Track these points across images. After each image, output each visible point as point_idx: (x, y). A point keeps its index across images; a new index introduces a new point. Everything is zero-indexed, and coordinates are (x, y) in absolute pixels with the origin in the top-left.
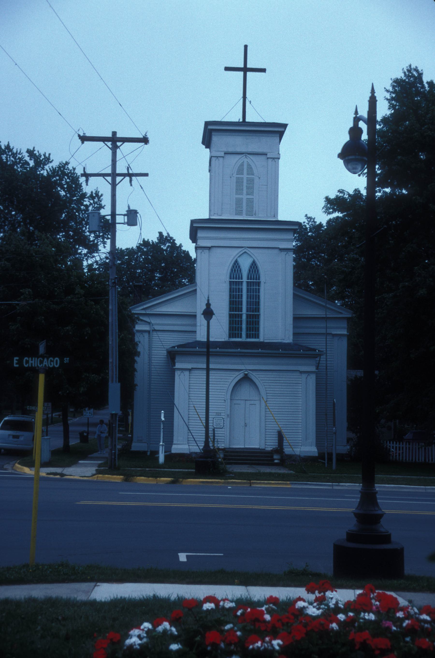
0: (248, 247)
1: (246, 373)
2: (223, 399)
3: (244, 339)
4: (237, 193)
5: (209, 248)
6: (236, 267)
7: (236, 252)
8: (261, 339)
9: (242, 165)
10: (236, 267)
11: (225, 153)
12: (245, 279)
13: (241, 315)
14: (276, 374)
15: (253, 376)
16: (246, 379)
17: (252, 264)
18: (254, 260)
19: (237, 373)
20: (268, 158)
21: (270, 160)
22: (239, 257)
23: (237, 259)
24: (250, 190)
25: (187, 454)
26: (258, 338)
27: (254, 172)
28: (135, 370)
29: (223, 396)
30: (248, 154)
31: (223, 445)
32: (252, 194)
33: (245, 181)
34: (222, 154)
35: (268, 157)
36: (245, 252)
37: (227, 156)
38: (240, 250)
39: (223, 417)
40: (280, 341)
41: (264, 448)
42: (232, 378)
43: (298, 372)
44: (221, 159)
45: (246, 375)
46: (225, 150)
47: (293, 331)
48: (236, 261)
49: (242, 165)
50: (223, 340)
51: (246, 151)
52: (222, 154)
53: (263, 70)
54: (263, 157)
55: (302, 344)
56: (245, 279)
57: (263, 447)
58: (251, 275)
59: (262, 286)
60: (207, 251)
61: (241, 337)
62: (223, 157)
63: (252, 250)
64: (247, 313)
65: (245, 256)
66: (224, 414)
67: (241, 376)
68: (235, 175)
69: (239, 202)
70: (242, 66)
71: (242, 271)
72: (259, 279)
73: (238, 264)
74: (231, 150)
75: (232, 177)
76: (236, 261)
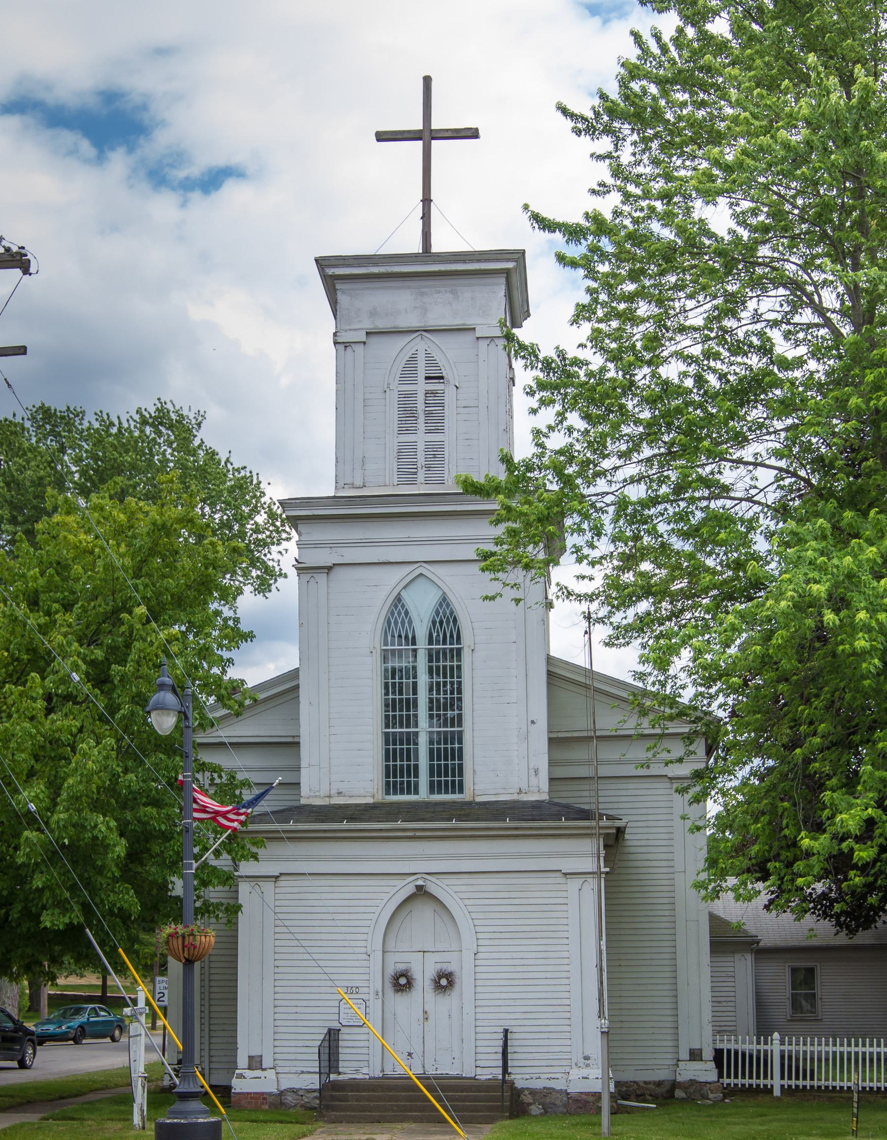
0: (425, 562)
1: (420, 883)
2: (363, 950)
3: (423, 794)
4: (403, 430)
5: (329, 569)
6: (399, 613)
7: (393, 578)
8: (466, 796)
9: (413, 359)
10: (399, 613)
11: (367, 333)
12: (422, 644)
13: (416, 734)
14: (501, 881)
15: (434, 887)
16: (421, 892)
17: (441, 605)
18: (444, 593)
19: (399, 883)
20: (478, 338)
21: (483, 344)
22: (404, 588)
23: (399, 594)
24: (435, 422)
25: (270, 1094)
26: (461, 791)
27: (443, 371)
28: (739, 926)
29: (363, 944)
30: (425, 331)
31: (365, 1070)
32: (439, 430)
33: (421, 398)
34: (363, 338)
35: (478, 334)
36: (421, 574)
37: (374, 340)
38: (407, 569)
39: (365, 997)
40: (515, 797)
41: (473, 1075)
42: (386, 897)
43: (558, 874)
44: (359, 349)
45: (419, 888)
46: (368, 325)
47: (550, 772)
48: (398, 599)
49: (413, 359)
50: (370, 800)
51: (422, 325)
52: (363, 338)
53: (427, 81)
54: (468, 338)
55: (582, 806)
56: (422, 644)
57: (468, 1072)
58: (438, 632)
59: (466, 655)
60: (322, 578)
61: (416, 792)
62: (364, 343)
63: (438, 570)
64: (430, 730)
65: (421, 584)
66: (366, 990)
67: (410, 890)
68: (395, 385)
69: (404, 452)
70: (418, 125)
71: (414, 624)
72: (459, 642)
73: (403, 606)
74: (382, 324)
75: (388, 390)
76: (398, 599)
